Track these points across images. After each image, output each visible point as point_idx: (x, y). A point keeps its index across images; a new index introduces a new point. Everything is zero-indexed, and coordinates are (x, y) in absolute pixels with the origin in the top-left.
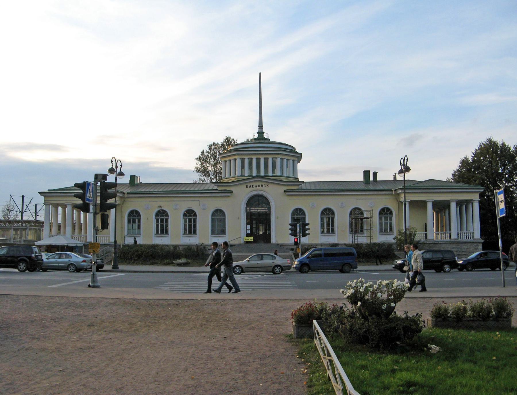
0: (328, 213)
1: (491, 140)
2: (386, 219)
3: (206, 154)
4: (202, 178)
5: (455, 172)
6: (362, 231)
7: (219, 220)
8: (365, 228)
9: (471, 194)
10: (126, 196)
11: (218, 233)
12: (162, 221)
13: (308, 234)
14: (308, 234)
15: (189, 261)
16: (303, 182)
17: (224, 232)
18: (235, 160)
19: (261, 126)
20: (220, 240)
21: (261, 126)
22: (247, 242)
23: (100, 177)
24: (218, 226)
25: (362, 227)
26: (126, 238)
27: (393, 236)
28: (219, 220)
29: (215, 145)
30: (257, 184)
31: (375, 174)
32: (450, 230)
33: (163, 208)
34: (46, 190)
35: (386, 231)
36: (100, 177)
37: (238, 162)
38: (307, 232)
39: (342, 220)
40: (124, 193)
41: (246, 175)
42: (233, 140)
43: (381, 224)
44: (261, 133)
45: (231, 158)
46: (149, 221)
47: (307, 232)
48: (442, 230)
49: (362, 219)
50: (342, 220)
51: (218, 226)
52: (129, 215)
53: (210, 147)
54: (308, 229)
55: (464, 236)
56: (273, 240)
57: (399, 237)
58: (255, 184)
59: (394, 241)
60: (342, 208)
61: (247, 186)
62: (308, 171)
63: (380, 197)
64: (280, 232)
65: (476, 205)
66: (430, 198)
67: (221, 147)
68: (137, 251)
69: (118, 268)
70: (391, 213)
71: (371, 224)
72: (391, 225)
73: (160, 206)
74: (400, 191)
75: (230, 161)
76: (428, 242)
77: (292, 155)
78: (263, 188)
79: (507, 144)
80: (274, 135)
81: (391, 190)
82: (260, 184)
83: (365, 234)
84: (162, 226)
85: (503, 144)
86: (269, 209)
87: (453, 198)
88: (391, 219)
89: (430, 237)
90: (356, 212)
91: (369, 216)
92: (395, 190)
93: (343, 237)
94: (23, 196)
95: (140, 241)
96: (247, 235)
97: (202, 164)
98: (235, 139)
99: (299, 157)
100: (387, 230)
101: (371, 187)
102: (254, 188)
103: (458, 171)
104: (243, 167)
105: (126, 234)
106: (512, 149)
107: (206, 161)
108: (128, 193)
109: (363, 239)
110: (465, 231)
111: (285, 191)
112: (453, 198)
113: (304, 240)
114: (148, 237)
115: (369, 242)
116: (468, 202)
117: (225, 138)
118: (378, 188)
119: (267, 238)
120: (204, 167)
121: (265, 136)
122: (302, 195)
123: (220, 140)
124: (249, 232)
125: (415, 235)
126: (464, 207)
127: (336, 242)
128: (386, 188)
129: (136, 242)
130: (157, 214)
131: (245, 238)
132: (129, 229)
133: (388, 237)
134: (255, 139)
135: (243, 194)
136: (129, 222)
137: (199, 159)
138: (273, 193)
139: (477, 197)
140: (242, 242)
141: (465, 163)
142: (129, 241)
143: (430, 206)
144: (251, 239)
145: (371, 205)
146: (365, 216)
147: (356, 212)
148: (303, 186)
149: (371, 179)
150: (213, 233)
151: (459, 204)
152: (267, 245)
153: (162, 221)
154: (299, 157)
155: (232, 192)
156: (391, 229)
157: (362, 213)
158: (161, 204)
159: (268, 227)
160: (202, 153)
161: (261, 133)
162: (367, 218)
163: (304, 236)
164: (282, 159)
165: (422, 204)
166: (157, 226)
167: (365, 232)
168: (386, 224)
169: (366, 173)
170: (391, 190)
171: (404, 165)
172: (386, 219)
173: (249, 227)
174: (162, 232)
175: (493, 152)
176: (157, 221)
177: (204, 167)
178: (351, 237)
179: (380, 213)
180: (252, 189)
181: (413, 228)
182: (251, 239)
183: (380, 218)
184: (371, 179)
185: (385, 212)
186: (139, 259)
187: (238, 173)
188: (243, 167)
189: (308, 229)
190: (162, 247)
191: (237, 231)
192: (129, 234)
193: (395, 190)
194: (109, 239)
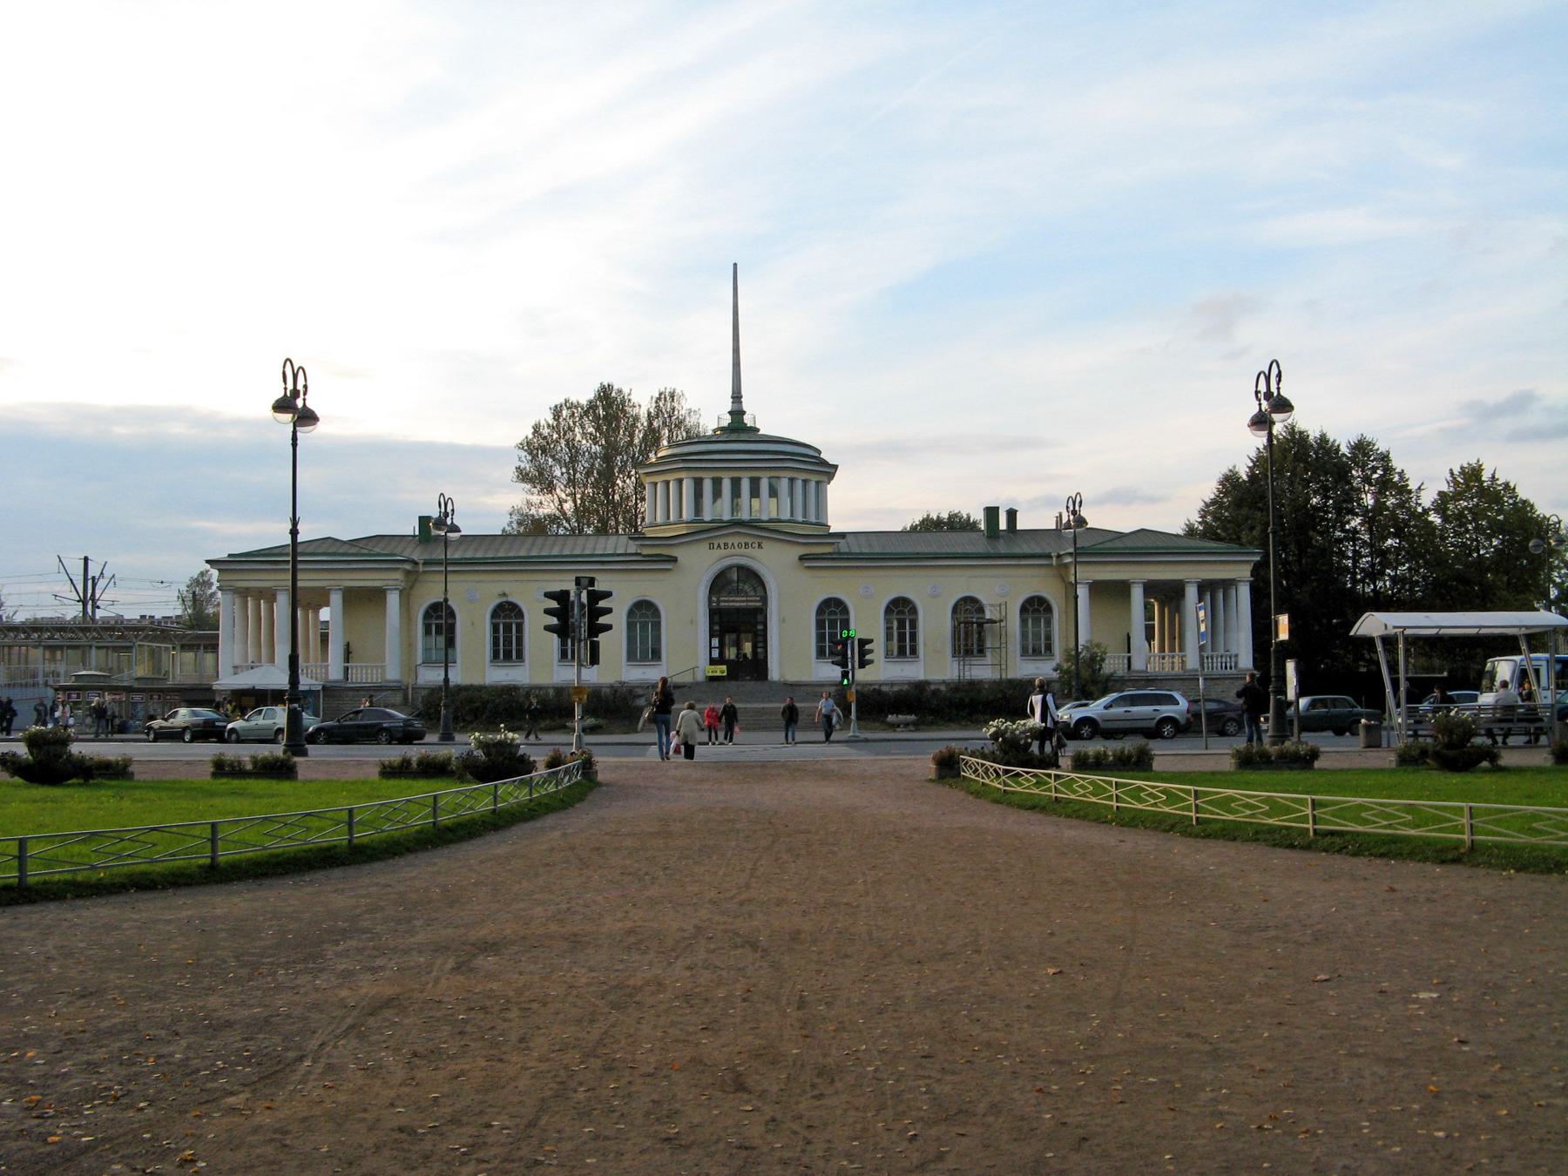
0: (901, 611)
1: (1293, 427)
2: (1036, 622)
3: (546, 432)
4: (535, 499)
5: (1207, 505)
6: (981, 651)
7: (644, 626)
8: (988, 644)
9: (1231, 567)
10: (421, 568)
11: (644, 658)
12: (508, 628)
13: (871, 662)
14: (871, 662)
15: (601, 722)
16: (842, 535)
17: (656, 655)
18: (680, 481)
19: (737, 397)
20: (651, 674)
21: (737, 397)
22: (712, 679)
23: (584, 582)
24: (644, 641)
25: (981, 641)
26: (421, 670)
27: (1053, 664)
28: (644, 626)
29: (571, 406)
30: (736, 540)
31: (1012, 515)
32: (1181, 650)
33: (510, 599)
34: (223, 555)
35: (1036, 652)
36: (584, 582)
37: (688, 487)
38: (602, 620)
39: (935, 625)
40: (416, 563)
41: (707, 517)
42: (620, 391)
43: (1024, 635)
44: (737, 413)
45: (671, 477)
46: (474, 630)
47: (602, 620)
48: (1172, 649)
49: (980, 625)
50: (935, 625)
51: (644, 641)
52: (427, 615)
53: (557, 412)
54: (871, 651)
55: (1217, 663)
56: (774, 673)
57: (1065, 666)
58: (730, 541)
59: (1055, 675)
60: (934, 597)
61: (711, 547)
62: (852, 506)
63: (1021, 572)
64: (792, 654)
65: (1244, 592)
66: (1137, 574)
67: (586, 413)
68: (471, 701)
69: (452, 739)
70: (1049, 609)
71: (1002, 635)
72: (1049, 637)
73: (505, 595)
74: (1069, 560)
75: (667, 483)
76: (1134, 676)
77: (813, 467)
78: (750, 550)
79: (1331, 437)
80: (768, 419)
81: (1049, 556)
82: (743, 540)
83: (989, 658)
84: (508, 641)
85: (1323, 439)
86: (764, 599)
87: (1191, 574)
88: (1049, 623)
89: (1138, 665)
90: (967, 609)
91: (996, 617)
92: (1059, 556)
93: (935, 664)
94: (86, 559)
95: (458, 677)
96: (713, 662)
97: (534, 457)
98: (626, 391)
99: (829, 471)
100: (1037, 648)
101: (1002, 548)
102: (729, 551)
103: (1213, 502)
104: (698, 495)
105: (419, 661)
106: (1344, 450)
107: (544, 452)
108: (426, 563)
109: (982, 671)
110: (1222, 652)
111: (802, 558)
112: (1191, 574)
113: (862, 675)
114: (475, 667)
115: (996, 676)
116: (1227, 585)
117: (597, 386)
118: (1017, 550)
119: (756, 668)
120: (541, 471)
121: (748, 420)
122: (948, 566)
123: (584, 394)
124: (716, 654)
125: (1103, 660)
126: (1221, 596)
127: (921, 677)
128: (1038, 550)
129: (446, 680)
130: (495, 614)
131: (704, 669)
132: (427, 650)
133: (1040, 664)
134: (722, 429)
135: (700, 564)
136: (427, 631)
137: (528, 446)
138: (775, 563)
139: (1244, 573)
140: (700, 677)
141: (1230, 482)
142: (431, 676)
143: (1137, 594)
144: (721, 670)
145: (1001, 592)
146: (988, 616)
147: (967, 609)
148: (843, 546)
149: (1003, 525)
150: (631, 657)
151: (1205, 587)
152: (758, 685)
153: (508, 628)
154: (829, 471)
155: (674, 560)
156: (1049, 648)
157: (981, 610)
158: (506, 588)
159: (761, 639)
160: (536, 429)
161: (737, 413)
162: (992, 622)
163: (862, 665)
164: (792, 480)
165: (1121, 590)
166: (914, 637)
167: (988, 654)
168: (1037, 636)
169: (992, 513)
170: (1049, 556)
171: (1074, 512)
172: (1036, 622)
173: (715, 642)
174: (508, 656)
175: (1297, 458)
176: (495, 628)
177: (541, 471)
178: (956, 665)
179: (1024, 609)
180: (723, 552)
181: (1098, 645)
182: (721, 670)
183: (1024, 622)
184: (1003, 525)
185: (1035, 608)
186: (476, 717)
187: (687, 514)
188: (698, 495)
189: (871, 651)
190: (509, 690)
191: (688, 652)
192: (427, 662)
193: (1059, 556)
194: (384, 672)
